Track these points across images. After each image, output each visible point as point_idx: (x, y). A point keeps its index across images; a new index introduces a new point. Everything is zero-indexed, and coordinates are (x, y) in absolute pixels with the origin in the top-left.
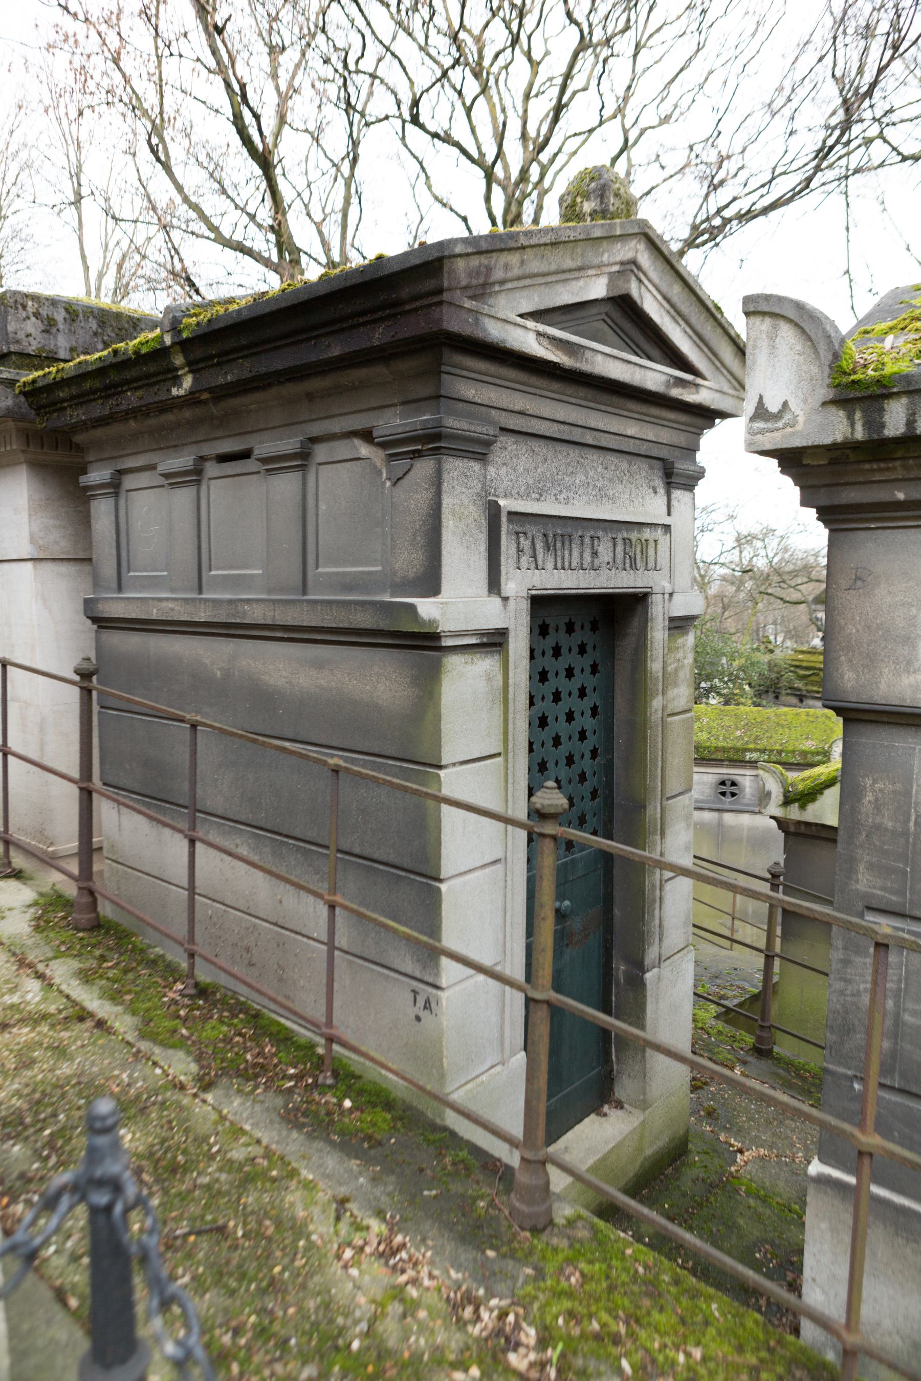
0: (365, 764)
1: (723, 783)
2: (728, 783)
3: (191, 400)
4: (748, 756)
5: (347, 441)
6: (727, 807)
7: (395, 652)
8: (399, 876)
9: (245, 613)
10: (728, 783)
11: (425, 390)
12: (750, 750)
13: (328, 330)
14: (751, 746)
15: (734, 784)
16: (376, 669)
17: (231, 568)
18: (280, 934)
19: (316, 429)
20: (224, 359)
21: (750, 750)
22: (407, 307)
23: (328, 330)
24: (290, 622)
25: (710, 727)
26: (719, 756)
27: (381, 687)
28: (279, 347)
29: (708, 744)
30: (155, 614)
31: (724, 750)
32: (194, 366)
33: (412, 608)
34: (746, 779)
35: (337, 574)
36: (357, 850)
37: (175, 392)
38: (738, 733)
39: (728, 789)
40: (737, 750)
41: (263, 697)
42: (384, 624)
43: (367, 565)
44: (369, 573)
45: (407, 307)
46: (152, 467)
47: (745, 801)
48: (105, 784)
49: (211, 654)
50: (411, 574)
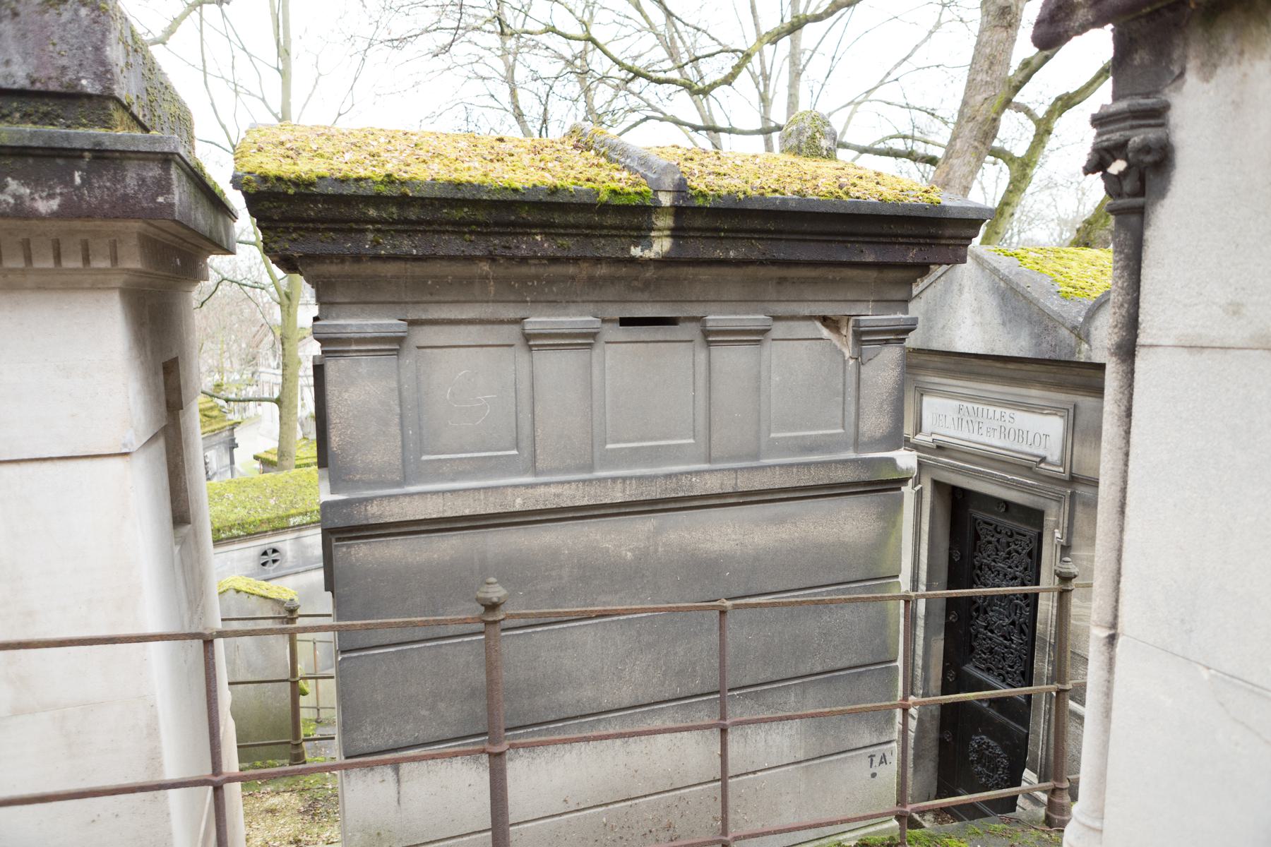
0: (829, 593)
1: (265, 553)
2: (270, 552)
3: (664, 262)
4: (292, 521)
5: (809, 323)
6: (272, 575)
7: (862, 498)
8: (860, 673)
9: (692, 486)
10: (270, 552)
11: (900, 295)
12: (293, 516)
13: (867, 239)
14: (293, 511)
15: (275, 551)
16: (843, 514)
17: (642, 439)
18: (649, 802)
19: (781, 309)
20: (713, 234)
21: (293, 516)
22: (943, 242)
23: (867, 239)
24: (758, 487)
25: (240, 502)
26: (265, 527)
27: (848, 527)
28: (805, 240)
29: (252, 519)
30: (518, 505)
31: (269, 521)
32: (677, 233)
33: (892, 461)
34: (285, 543)
35: (796, 438)
36: (819, 669)
37: (636, 252)
38: (272, 502)
39: (269, 557)
40: (281, 518)
41: (704, 568)
42: (865, 476)
43: (826, 427)
44: (831, 435)
45: (943, 242)
46: (519, 321)
47: (288, 564)
48: (347, 758)
49: (620, 540)
50: (878, 434)
